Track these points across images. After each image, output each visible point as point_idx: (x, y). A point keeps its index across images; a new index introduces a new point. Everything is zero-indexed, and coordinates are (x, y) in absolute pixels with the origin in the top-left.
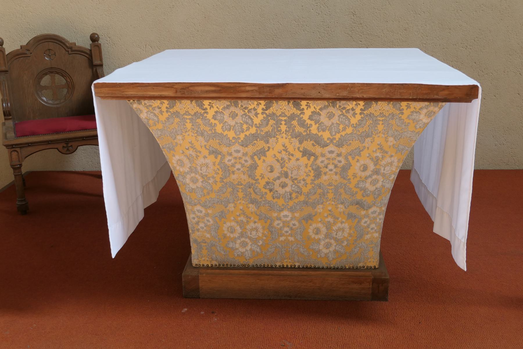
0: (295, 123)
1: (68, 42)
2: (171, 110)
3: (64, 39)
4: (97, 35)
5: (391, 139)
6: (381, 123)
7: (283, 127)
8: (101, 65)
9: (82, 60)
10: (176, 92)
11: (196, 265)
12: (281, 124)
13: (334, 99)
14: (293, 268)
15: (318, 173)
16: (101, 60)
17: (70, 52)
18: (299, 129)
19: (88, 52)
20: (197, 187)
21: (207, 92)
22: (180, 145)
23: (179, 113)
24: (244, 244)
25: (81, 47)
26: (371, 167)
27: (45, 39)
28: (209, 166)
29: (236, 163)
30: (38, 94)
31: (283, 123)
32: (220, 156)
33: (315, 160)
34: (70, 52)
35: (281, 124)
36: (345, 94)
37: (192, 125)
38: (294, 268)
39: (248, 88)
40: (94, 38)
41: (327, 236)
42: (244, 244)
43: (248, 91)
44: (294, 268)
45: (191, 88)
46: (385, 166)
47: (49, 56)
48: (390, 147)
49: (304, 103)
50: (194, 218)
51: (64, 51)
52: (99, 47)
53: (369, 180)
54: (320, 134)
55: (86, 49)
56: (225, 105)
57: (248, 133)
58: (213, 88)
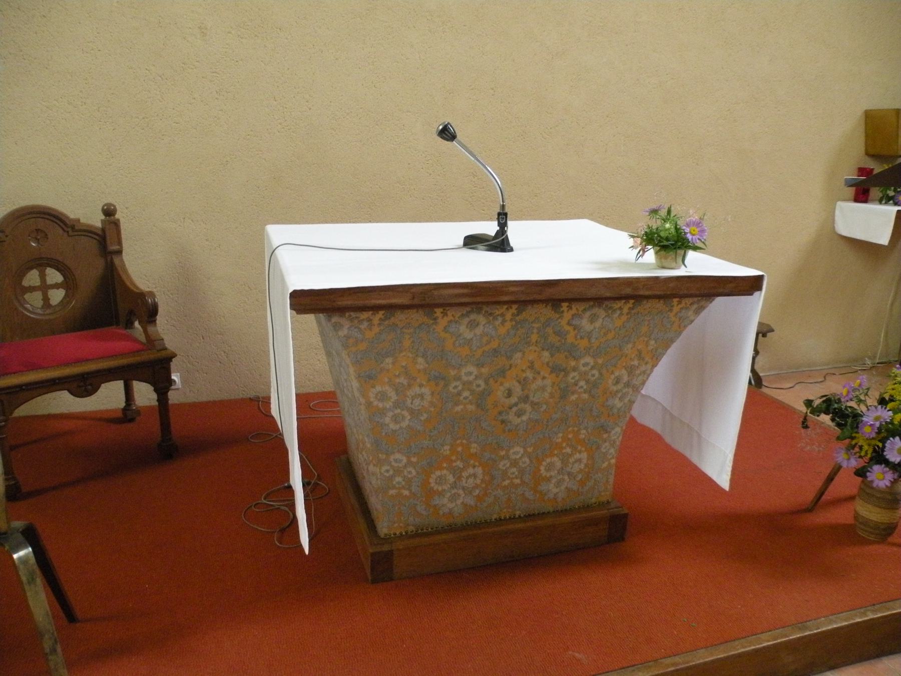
0: (549, 330)
1: (68, 217)
2: (387, 322)
3: (62, 214)
4: (115, 206)
5: (420, 360)
6: (407, 336)
7: (534, 337)
8: (119, 252)
9: (91, 245)
10: (413, 298)
11: (386, 535)
12: (532, 333)
13: (523, 301)
14: (512, 519)
15: (564, 394)
16: (120, 243)
17: (71, 233)
18: (553, 339)
19: (100, 233)
20: (401, 428)
21: (463, 295)
22: (388, 370)
23: (397, 325)
24: (453, 498)
25: (88, 226)
26: (518, 390)
27: (40, 213)
28: (425, 397)
29: (463, 389)
30: (19, 301)
31: (535, 331)
32: (442, 383)
33: (446, 385)
34: (71, 233)
35: (532, 333)
36: (628, 291)
37: (413, 342)
38: (514, 518)
39: (512, 289)
40: (109, 212)
41: (397, 405)
42: (453, 498)
43: (513, 292)
44: (514, 518)
45: (436, 293)
46: (413, 399)
47: (37, 240)
48: (419, 371)
49: (438, 311)
50: (387, 471)
51: (61, 231)
52: (116, 224)
53: (515, 409)
54: (576, 343)
55: (96, 228)
56: (465, 312)
57: (486, 348)
58: (465, 291)
